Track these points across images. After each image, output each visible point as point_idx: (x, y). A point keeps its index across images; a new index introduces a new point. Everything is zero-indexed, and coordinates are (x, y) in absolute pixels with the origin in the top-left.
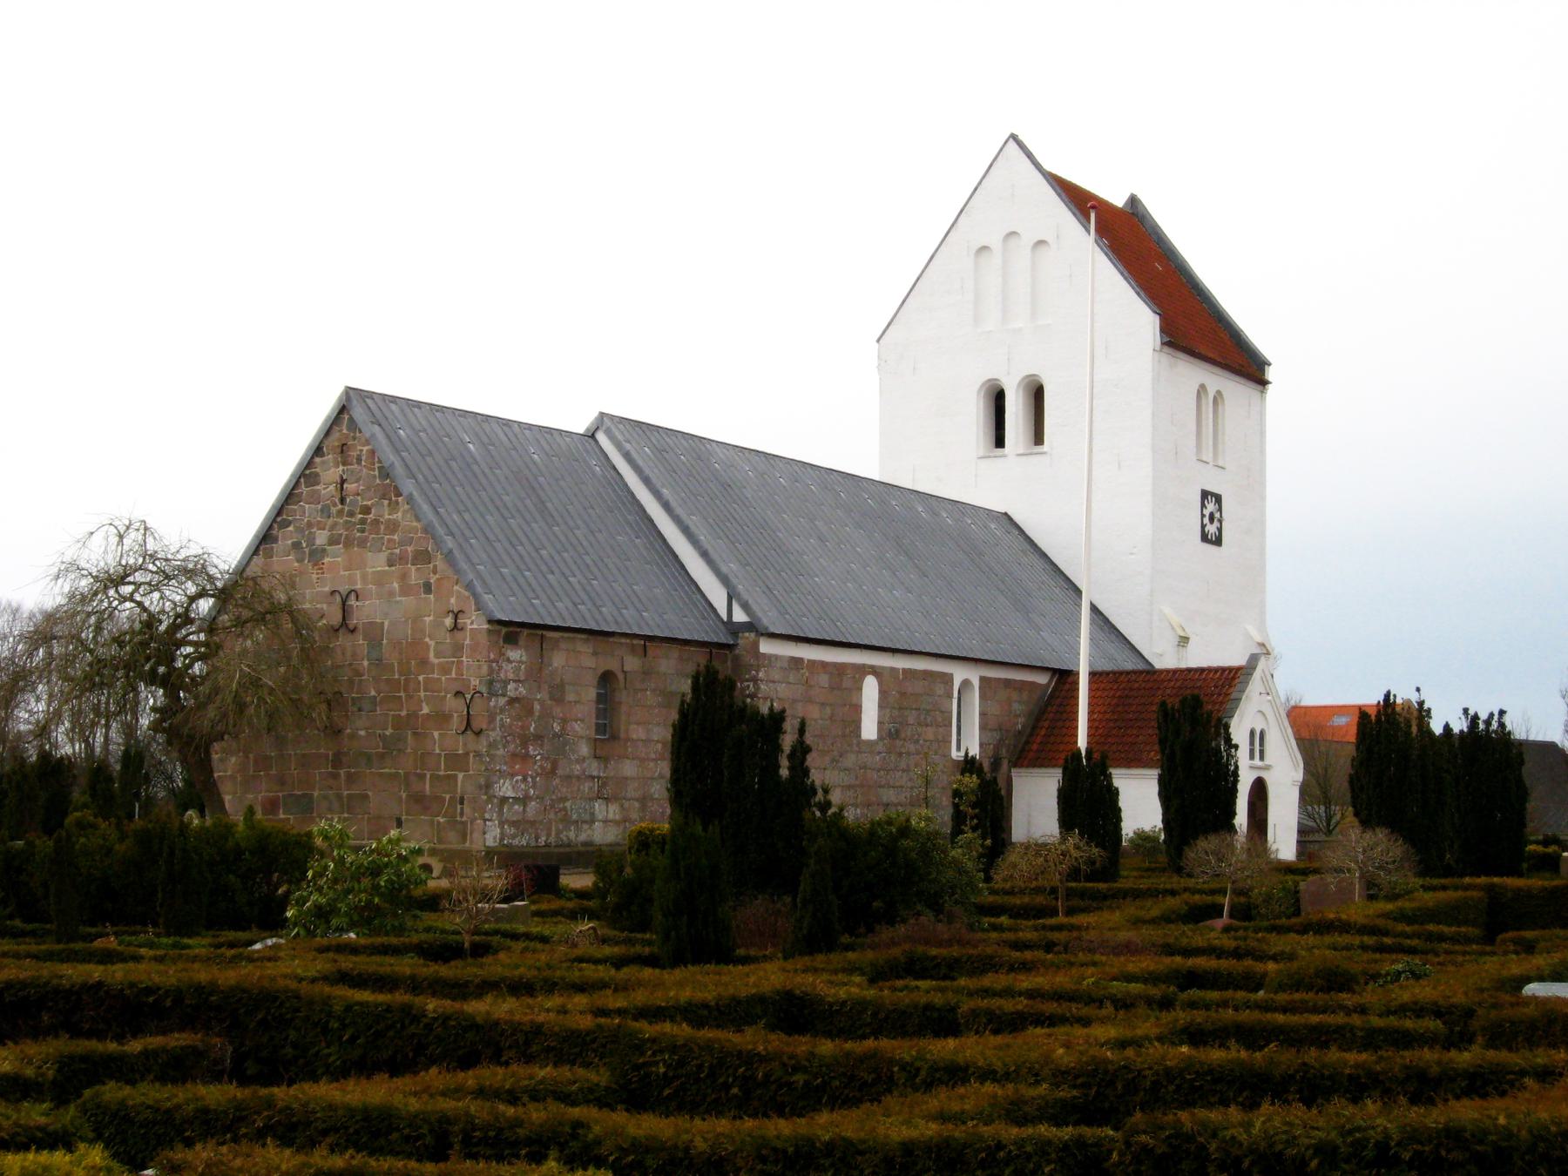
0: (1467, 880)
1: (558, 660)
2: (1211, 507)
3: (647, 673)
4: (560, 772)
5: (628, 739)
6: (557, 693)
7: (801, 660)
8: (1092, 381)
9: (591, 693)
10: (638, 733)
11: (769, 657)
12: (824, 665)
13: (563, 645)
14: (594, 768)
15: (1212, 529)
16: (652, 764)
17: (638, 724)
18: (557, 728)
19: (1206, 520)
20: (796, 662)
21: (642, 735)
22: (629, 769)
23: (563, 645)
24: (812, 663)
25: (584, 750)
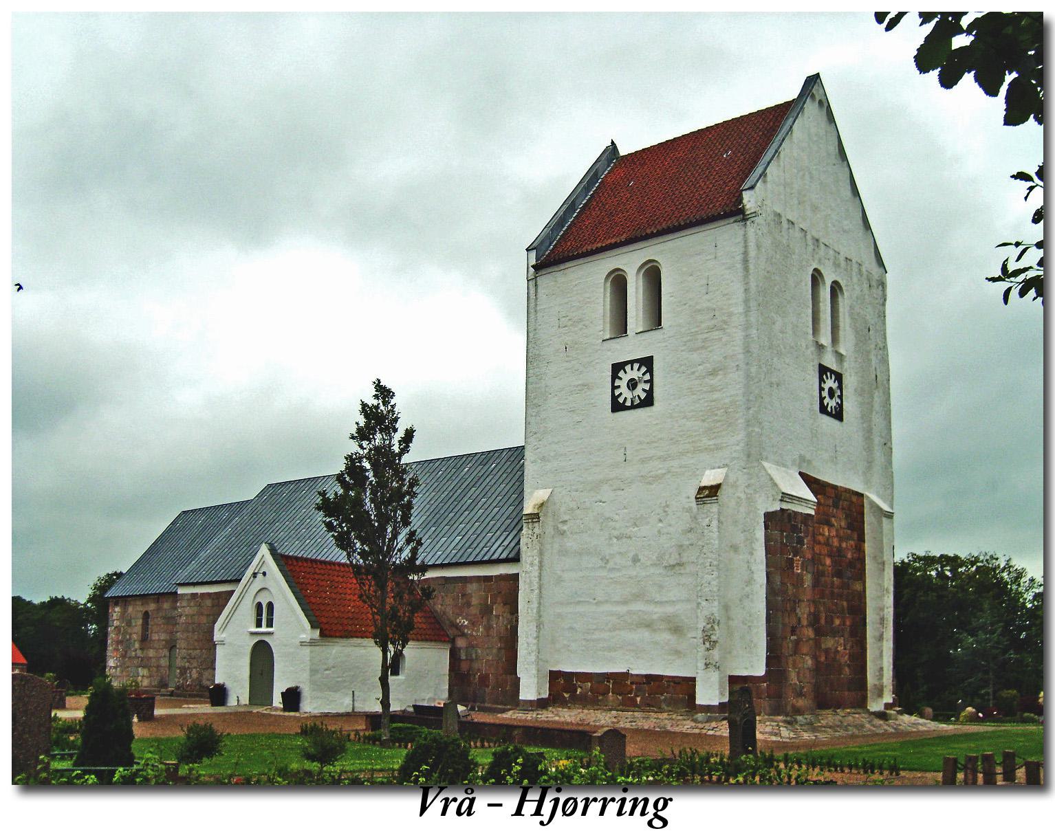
0: (988, 724)
1: (130, 609)
2: (830, 383)
3: (158, 609)
4: (128, 655)
5: (151, 640)
6: (129, 624)
7: (197, 594)
8: (746, 269)
9: (140, 622)
10: (155, 637)
11: (182, 595)
12: (209, 594)
13: (132, 602)
14: (139, 653)
15: (831, 403)
16: (161, 651)
17: (155, 633)
18: (128, 637)
19: (825, 394)
20: (194, 595)
21: (157, 638)
22: (151, 653)
23: (132, 602)
24: (203, 594)
25: (137, 645)
